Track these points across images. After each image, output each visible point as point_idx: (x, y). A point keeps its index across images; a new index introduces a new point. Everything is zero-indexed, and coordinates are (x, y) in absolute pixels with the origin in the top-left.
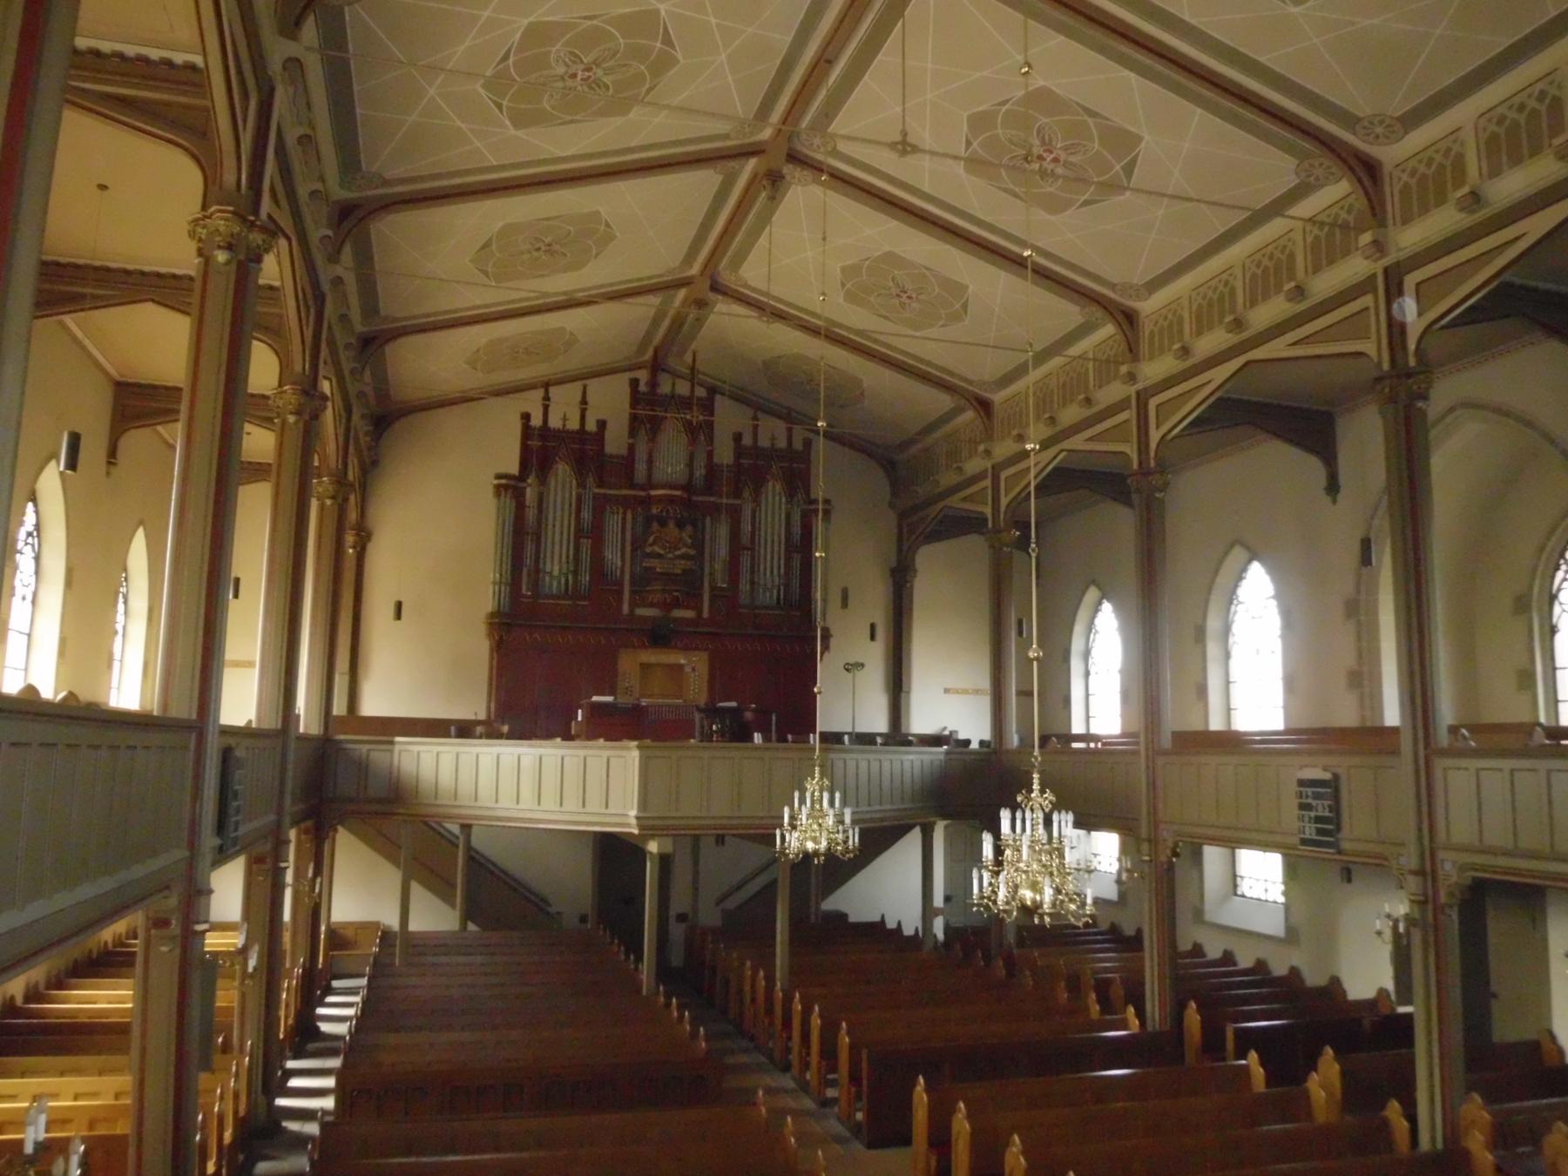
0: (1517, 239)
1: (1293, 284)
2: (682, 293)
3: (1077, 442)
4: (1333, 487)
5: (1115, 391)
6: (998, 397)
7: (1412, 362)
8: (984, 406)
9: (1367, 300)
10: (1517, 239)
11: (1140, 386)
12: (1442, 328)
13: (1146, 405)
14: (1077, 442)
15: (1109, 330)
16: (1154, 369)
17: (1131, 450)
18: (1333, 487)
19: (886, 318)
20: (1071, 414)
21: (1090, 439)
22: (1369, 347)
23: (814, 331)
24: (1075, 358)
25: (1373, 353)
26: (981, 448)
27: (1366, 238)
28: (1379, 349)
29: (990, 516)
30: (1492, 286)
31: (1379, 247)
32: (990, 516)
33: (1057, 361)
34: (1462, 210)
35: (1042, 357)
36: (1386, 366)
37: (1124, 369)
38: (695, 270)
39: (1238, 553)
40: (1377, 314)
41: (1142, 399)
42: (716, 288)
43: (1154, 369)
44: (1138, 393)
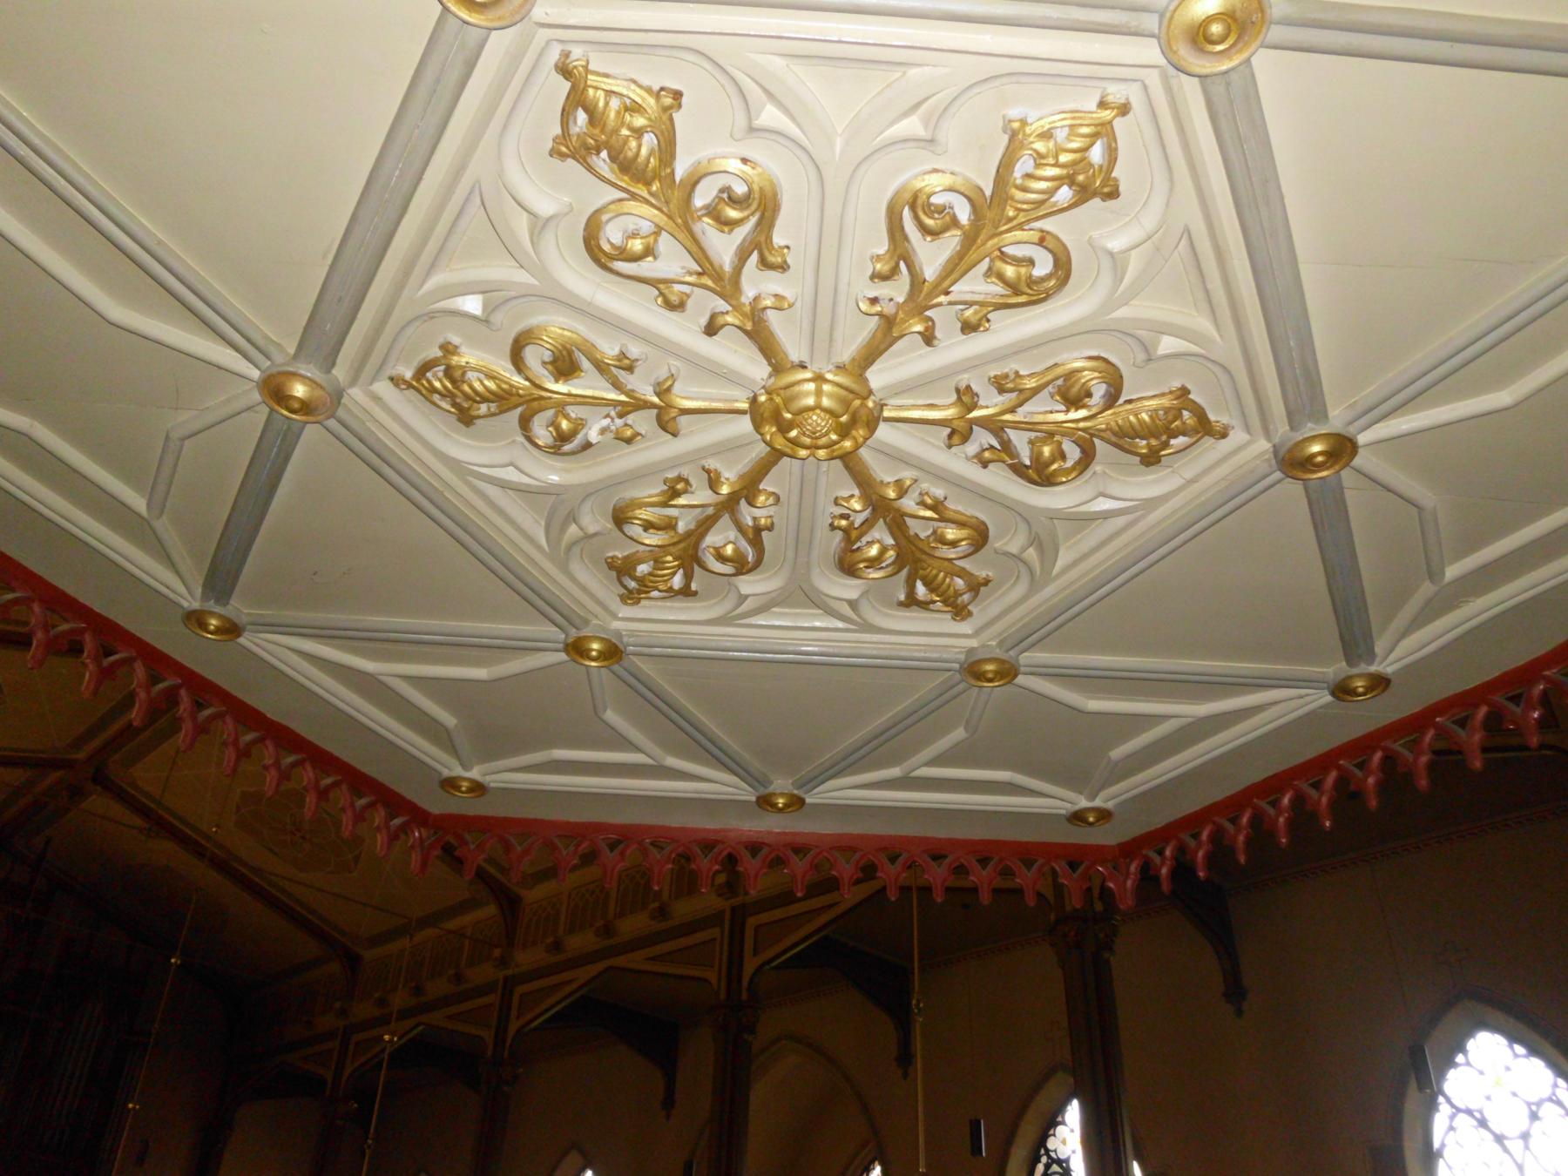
0: (831, 906)
1: (656, 904)
2: (56, 775)
3: (437, 1018)
4: (669, 1102)
5: (484, 973)
6: (369, 955)
7: (744, 996)
8: (352, 961)
9: (714, 932)
10: (831, 906)
11: (509, 972)
12: (777, 968)
13: (743, 924)
14: (437, 1018)
15: (491, 910)
16: (526, 958)
17: (488, 1035)
18: (669, 1102)
19: (271, 850)
20: (438, 987)
21: (449, 1017)
22: (712, 976)
23: (199, 852)
24: (450, 932)
25: (714, 980)
26: (338, 1005)
27: (497, 952)
28: (719, 980)
29: (330, 1080)
30: (568, 1001)
31: (503, 962)
32: (330, 1080)
33: (429, 932)
34: (720, 895)
35: (424, 922)
36: (723, 996)
37: (497, 952)
38: (81, 755)
39: (574, 1158)
40: (722, 944)
41: (510, 984)
42: (101, 780)
43: (526, 958)
44: (506, 979)
